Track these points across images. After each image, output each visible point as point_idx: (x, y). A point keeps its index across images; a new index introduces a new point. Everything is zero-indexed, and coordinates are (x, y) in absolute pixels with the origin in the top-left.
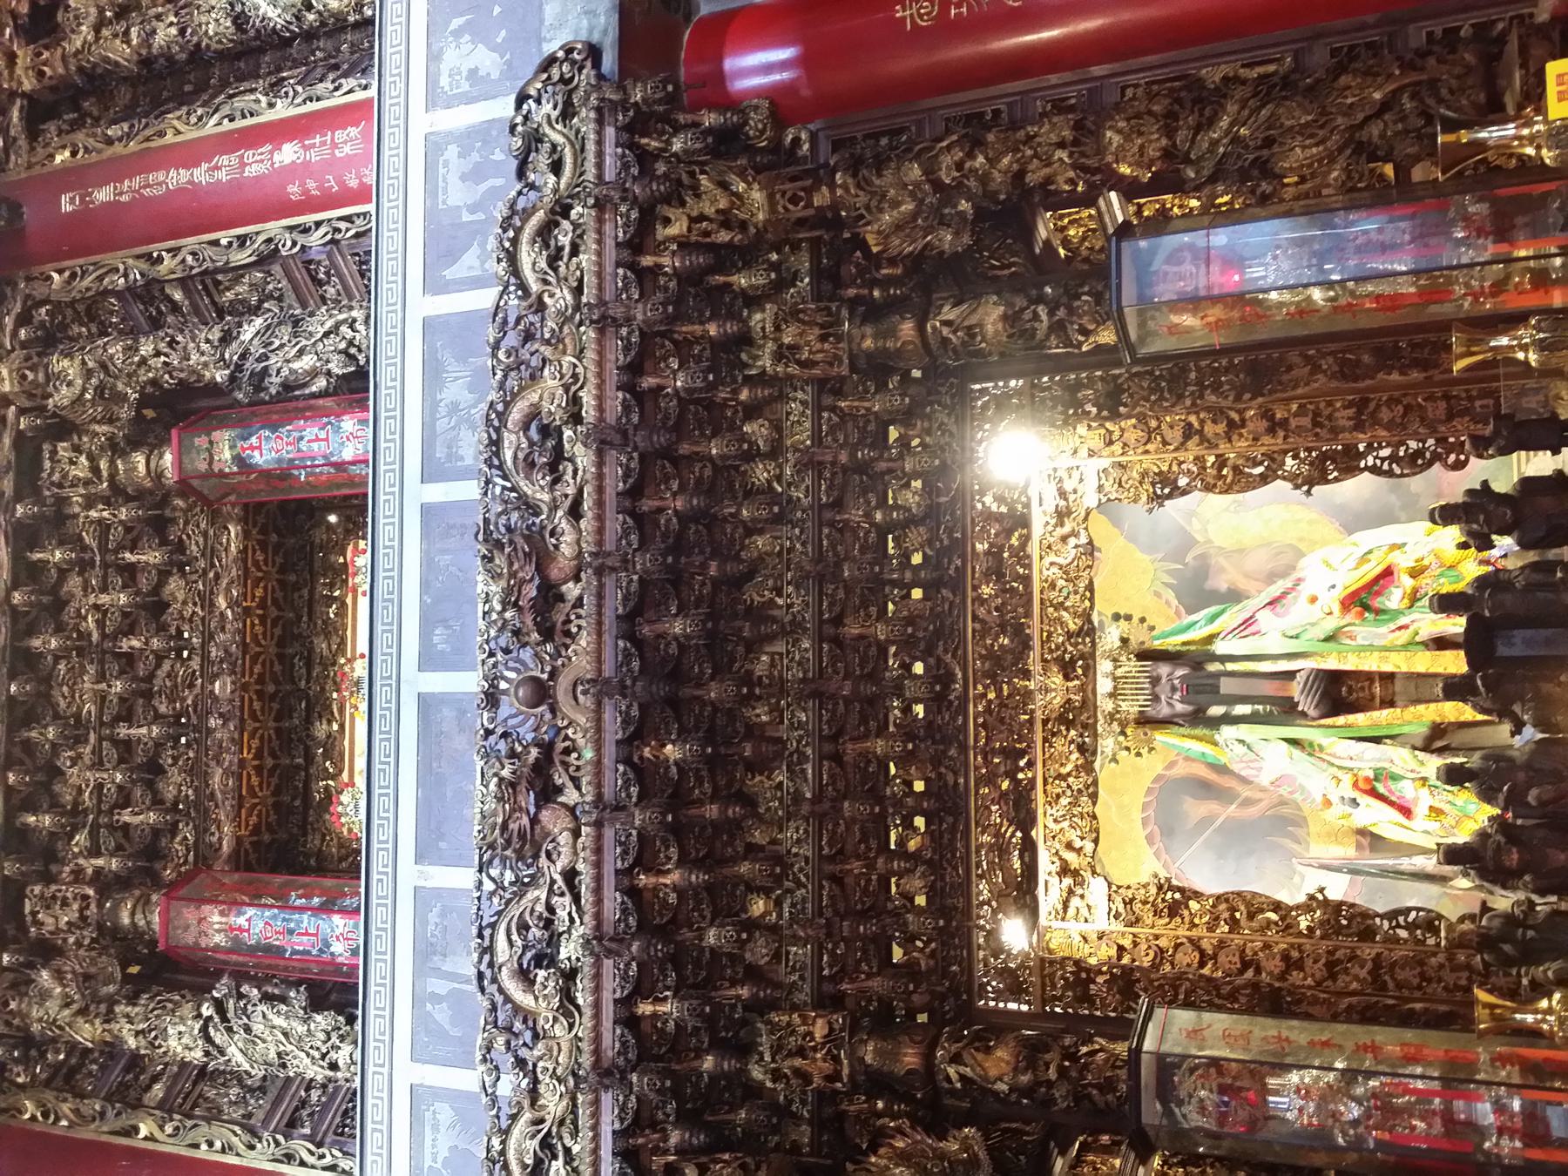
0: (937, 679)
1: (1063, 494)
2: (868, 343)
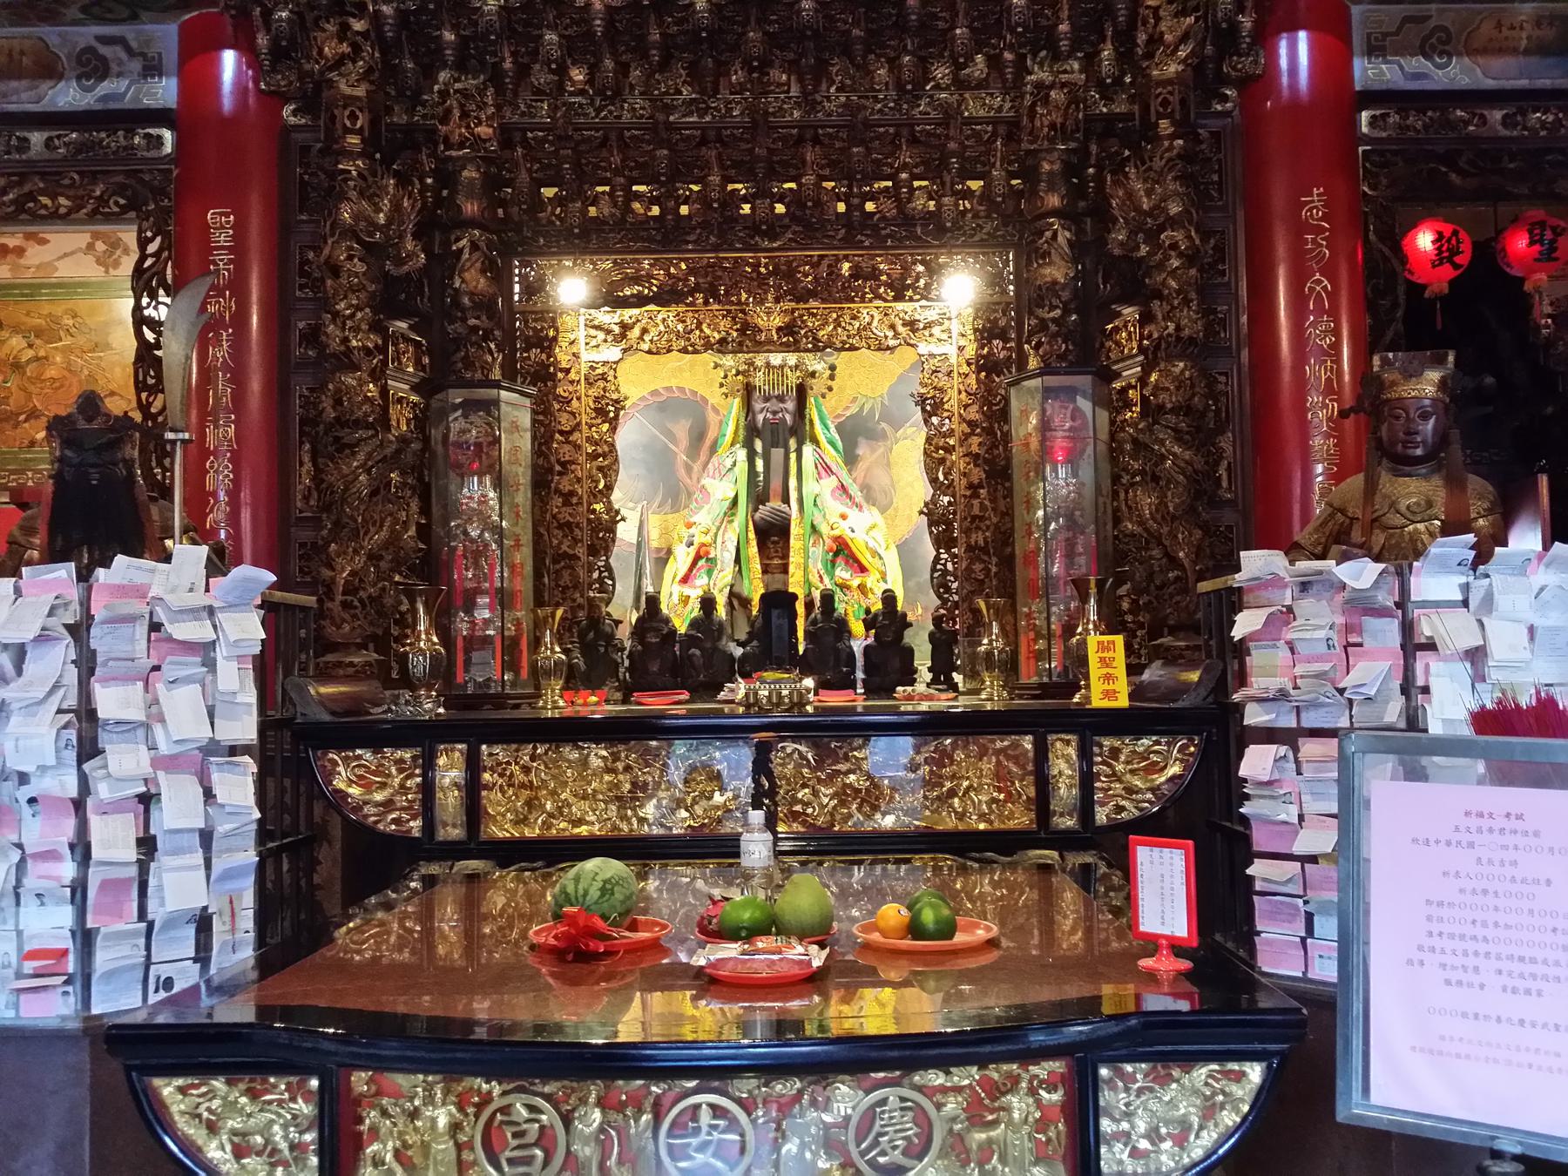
0: (771, 227)
1: (928, 326)
2: (1046, 167)
